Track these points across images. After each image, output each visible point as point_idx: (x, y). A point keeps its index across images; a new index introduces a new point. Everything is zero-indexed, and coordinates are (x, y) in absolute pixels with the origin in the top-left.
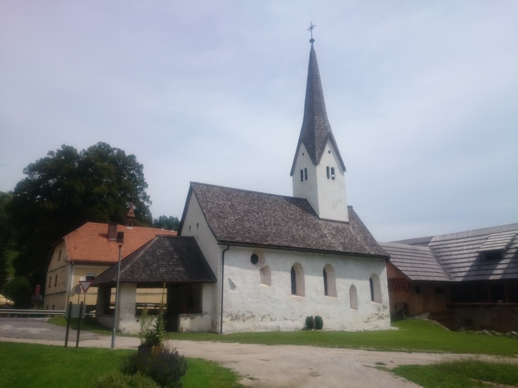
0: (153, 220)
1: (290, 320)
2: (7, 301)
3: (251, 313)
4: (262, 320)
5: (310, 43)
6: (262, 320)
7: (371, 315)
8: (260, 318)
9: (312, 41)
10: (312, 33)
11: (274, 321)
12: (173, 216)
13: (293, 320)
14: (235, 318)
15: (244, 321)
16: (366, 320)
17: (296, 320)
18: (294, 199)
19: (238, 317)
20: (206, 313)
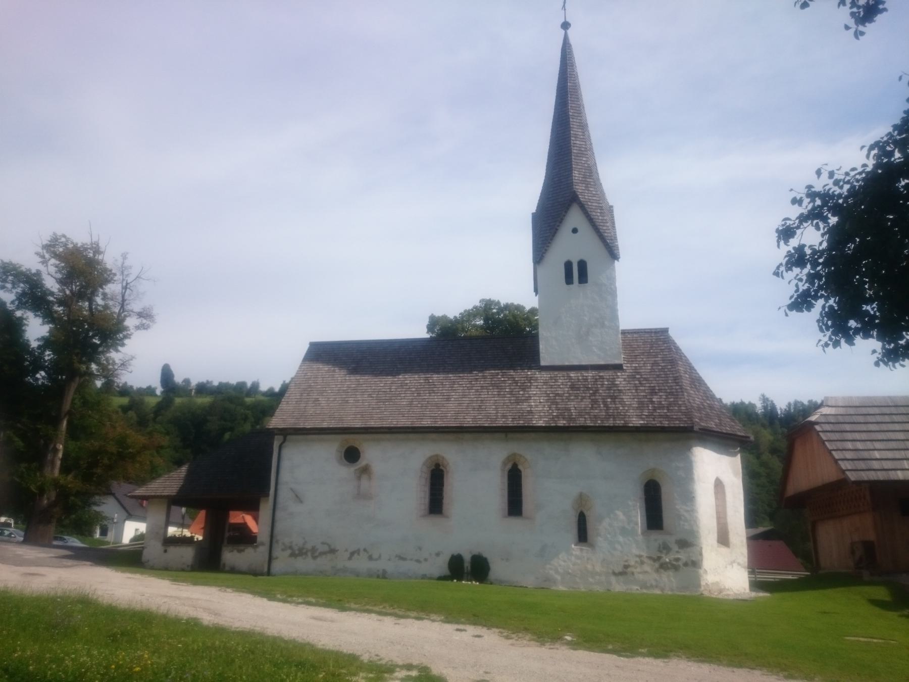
0: (779, 412)
1: (411, 560)
2: (182, 532)
3: (329, 546)
4: (350, 558)
5: (563, 30)
6: (350, 558)
7: (638, 559)
8: (347, 555)
9: (566, 26)
10: (566, 11)
11: (376, 560)
12: (814, 400)
13: (418, 561)
14: (299, 553)
15: (315, 558)
16: (619, 569)
17: (426, 560)
18: (645, 332)
19: (304, 551)
20: (262, 544)
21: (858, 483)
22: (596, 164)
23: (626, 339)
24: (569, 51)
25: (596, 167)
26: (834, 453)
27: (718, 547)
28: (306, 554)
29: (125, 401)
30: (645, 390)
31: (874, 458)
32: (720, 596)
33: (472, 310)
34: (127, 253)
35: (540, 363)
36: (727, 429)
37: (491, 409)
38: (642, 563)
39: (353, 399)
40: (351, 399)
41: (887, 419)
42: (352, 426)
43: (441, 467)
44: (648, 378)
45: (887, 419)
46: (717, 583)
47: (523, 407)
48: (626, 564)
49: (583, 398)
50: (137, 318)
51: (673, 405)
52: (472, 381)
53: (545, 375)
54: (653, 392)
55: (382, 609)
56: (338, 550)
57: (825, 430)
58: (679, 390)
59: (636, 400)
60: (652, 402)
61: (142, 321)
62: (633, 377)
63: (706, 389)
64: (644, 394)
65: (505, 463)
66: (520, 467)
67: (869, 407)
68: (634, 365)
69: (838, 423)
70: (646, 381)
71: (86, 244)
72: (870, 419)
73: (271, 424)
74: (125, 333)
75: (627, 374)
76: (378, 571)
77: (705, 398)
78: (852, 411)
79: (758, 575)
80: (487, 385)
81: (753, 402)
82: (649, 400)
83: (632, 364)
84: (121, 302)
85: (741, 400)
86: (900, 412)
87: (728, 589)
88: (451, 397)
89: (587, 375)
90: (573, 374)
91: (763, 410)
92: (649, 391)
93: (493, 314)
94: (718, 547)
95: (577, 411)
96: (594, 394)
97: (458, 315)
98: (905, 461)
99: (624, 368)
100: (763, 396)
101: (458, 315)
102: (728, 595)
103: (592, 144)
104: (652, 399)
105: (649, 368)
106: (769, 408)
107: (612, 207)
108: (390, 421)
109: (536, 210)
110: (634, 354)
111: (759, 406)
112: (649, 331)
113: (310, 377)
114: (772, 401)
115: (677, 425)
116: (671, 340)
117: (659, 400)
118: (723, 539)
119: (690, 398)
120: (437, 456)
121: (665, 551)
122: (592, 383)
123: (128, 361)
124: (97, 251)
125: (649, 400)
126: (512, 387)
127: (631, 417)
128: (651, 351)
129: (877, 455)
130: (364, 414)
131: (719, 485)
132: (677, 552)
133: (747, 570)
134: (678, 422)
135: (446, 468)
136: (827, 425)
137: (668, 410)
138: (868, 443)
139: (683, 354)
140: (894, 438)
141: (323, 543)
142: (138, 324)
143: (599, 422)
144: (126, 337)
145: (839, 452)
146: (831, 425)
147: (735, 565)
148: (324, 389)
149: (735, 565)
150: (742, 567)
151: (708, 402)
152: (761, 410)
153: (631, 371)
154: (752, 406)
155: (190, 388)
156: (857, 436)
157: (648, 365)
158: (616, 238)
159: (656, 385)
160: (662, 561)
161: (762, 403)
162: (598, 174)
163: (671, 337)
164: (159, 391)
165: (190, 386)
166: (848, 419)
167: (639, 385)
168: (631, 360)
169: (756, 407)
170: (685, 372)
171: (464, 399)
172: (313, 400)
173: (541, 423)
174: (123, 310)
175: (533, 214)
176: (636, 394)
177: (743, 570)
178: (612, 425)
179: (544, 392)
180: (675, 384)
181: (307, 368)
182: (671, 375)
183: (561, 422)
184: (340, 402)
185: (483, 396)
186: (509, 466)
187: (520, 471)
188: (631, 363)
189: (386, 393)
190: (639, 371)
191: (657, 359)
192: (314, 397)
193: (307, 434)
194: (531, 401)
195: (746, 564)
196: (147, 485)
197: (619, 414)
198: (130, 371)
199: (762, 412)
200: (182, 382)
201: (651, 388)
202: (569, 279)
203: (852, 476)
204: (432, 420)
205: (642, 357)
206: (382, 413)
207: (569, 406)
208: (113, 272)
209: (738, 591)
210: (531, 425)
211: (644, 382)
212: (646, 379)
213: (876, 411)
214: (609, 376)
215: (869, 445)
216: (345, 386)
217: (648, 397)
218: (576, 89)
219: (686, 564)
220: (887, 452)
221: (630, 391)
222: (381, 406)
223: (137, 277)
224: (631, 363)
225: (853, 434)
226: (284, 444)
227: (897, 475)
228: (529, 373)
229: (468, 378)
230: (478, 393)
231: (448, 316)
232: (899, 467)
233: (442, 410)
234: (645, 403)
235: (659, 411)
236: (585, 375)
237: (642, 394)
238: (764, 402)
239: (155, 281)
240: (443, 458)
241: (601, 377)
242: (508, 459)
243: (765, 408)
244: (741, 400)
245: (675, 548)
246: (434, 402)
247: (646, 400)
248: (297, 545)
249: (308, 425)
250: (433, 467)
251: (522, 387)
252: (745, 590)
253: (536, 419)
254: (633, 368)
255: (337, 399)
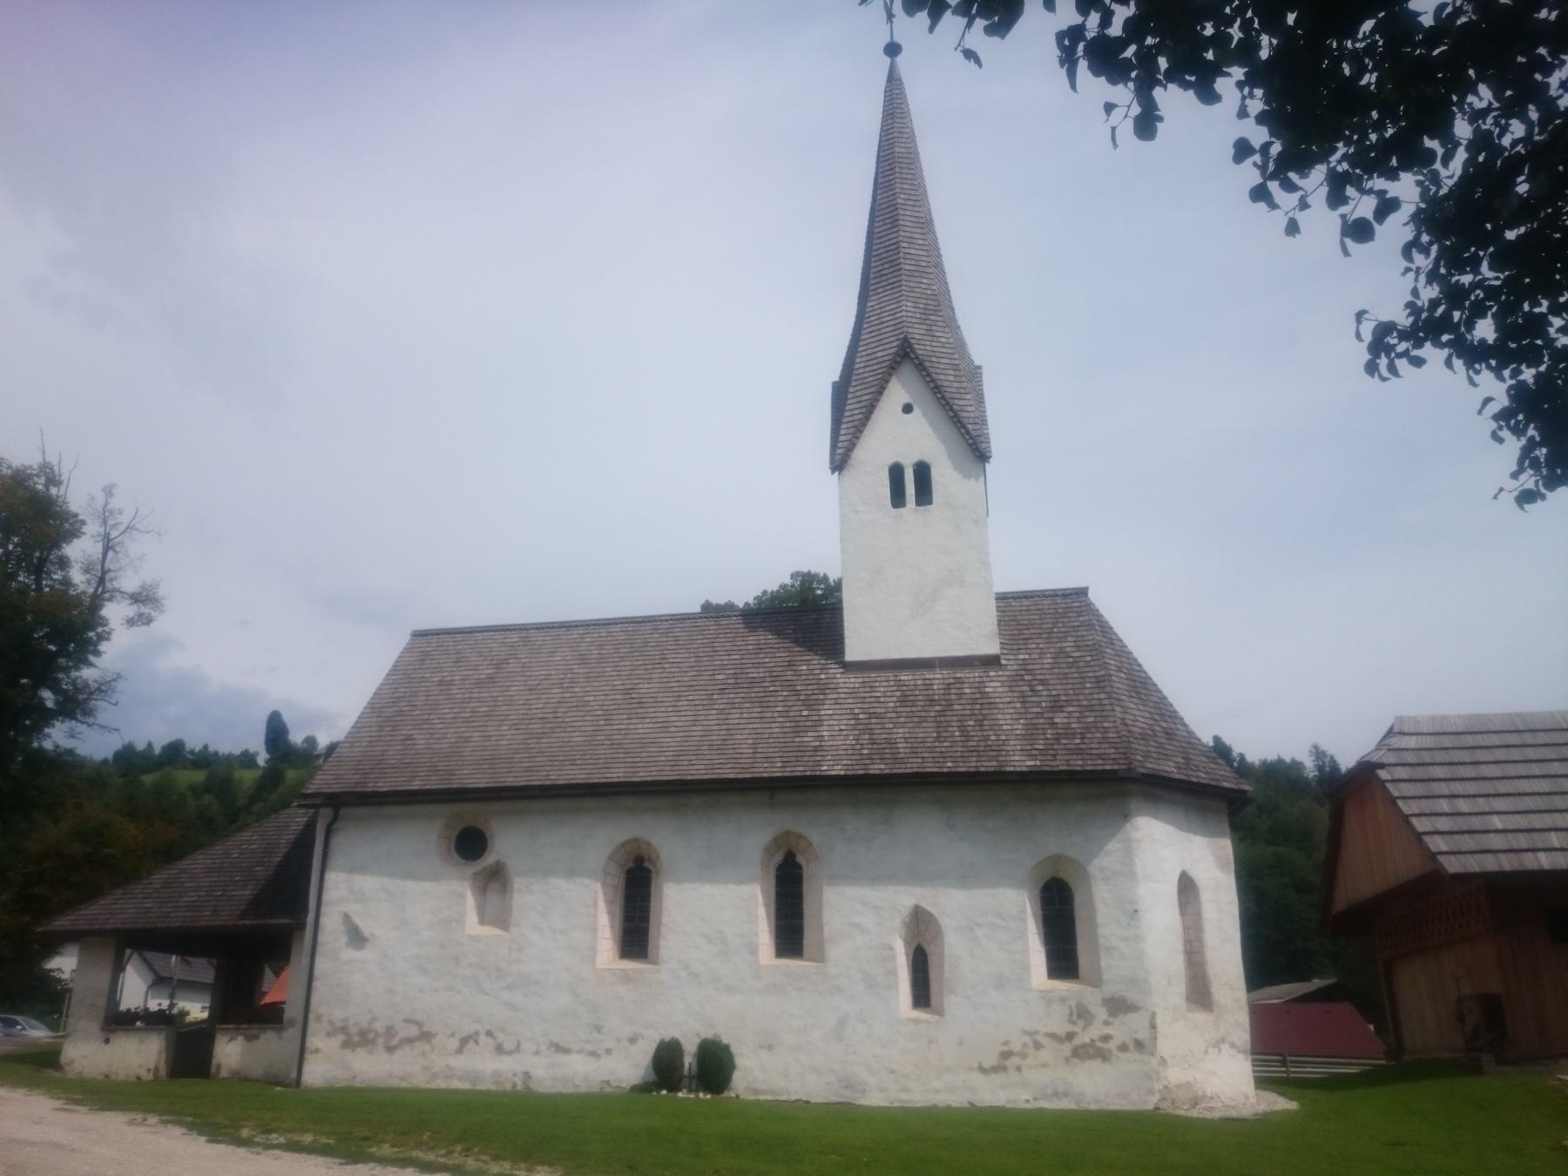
3: (419, 1024)
6: (460, 1051)
7: (1028, 1039)
8: (454, 1044)
11: (510, 1053)
13: (593, 1054)
14: (358, 1039)
15: (390, 1049)
16: (990, 1060)
17: (609, 1051)
19: (371, 1036)
21: (1462, 878)
22: (949, 291)
23: (1009, 609)
24: (898, 92)
25: (949, 296)
26: (1414, 821)
27: (1189, 1010)
28: (373, 1041)
29: (199, 777)
30: (1041, 702)
31: (1493, 828)
32: (1194, 1113)
33: (778, 591)
34: (114, 485)
35: (843, 656)
36: (1202, 777)
37: (745, 746)
38: (1038, 1046)
39: (480, 734)
40: (475, 734)
41: (1516, 754)
42: (471, 786)
43: (646, 864)
44: (1046, 679)
45: (1516, 754)
46: (1189, 1085)
47: (806, 739)
48: (1006, 1048)
49: (924, 720)
50: (131, 604)
51: (1093, 730)
52: (713, 694)
53: (853, 680)
54: (1056, 706)
55: (442, 1156)
56: (437, 1034)
57: (1396, 777)
58: (1106, 702)
59: (1022, 721)
60: (1053, 724)
61: (139, 609)
62: (1017, 678)
63: (1158, 700)
64: (1038, 710)
65: (769, 852)
66: (800, 859)
67: (1481, 733)
68: (1021, 657)
69: (1423, 764)
70: (1043, 685)
71: (30, 467)
72: (1481, 755)
73: (311, 786)
74: (100, 630)
75: (1007, 673)
76: (515, 1075)
77: (1157, 717)
78: (1447, 741)
79: (1292, 1067)
80: (740, 700)
81: (1299, 758)
82: (1047, 721)
83: (1018, 654)
84: (99, 575)
85: (1279, 756)
86: (1541, 742)
87: (1212, 1098)
88: (670, 724)
89: (932, 676)
90: (905, 677)
91: (1317, 773)
92: (1049, 704)
93: (815, 596)
94: (1189, 1010)
95: (909, 745)
96: (942, 713)
97: (751, 601)
98: (1553, 834)
99: (1003, 662)
100: (1316, 747)
101: (751, 601)
102: (1211, 1109)
103: (941, 256)
104: (1052, 718)
105: (1050, 661)
106: (1328, 769)
107: (980, 367)
108: (544, 773)
109: (840, 377)
110: (1022, 637)
111: (1309, 763)
112: (1051, 593)
113: (401, 695)
114: (1332, 757)
115: (1100, 768)
116: (1092, 610)
117: (1066, 720)
118: (1199, 993)
119: (1127, 716)
120: (637, 840)
121: (1081, 1023)
122: (942, 692)
123: (109, 682)
124: (53, 480)
125: (1047, 721)
126: (789, 704)
127: (1011, 753)
128: (1055, 630)
129: (1497, 822)
130: (497, 761)
131: (1187, 887)
132: (1106, 1023)
133: (1250, 1057)
134: (1100, 762)
135: (655, 866)
136: (1400, 768)
137: (1083, 738)
138: (1481, 800)
139: (1116, 635)
140: (1530, 791)
141: (407, 1021)
142: (131, 614)
143: (950, 764)
144: (101, 638)
145: (1423, 818)
146: (1407, 768)
147: (1225, 1047)
148: (426, 717)
149: (1225, 1047)
150: (1239, 1052)
151: (1164, 725)
152: (1313, 771)
153: (1015, 667)
154: (1296, 766)
155: (316, 753)
156: (1457, 788)
157: (1049, 656)
158: (984, 422)
159: (1061, 692)
160: (1078, 1041)
161: (1314, 761)
162: (953, 309)
163: (1094, 605)
164: (262, 759)
165: (316, 749)
166: (1440, 757)
167: (1030, 694)
168: (1015, 647)
169: (1305, 768)
170: (1120, 667)
171: (694, 728)
172: (402, 737)
173: (838, 770)
174: (103, 589)
175: (834, 383)
176: (1022, 711)
177: (1242, 1056)
178: (973, 770)
179: (848, 711)
180: (1097, 690)
181: (401, 679)
182: (1091, 674)
183: (876, 767)
184: (453, 740)
185: (731, 722)
186: (779, 858)
187: (800, 867)
188: (1016, 652)
189: (545, 721)
190: (1030, 667)
191: (1065, 644)
192: (404, 732)
193: (380, 804)
194: (823, 728)
195: (1248, 1046)
196: (67, 915)
197: (988, 748)
198: (114, 702)
199: (1316, 776)
200: (302, 743)
201: (1052, 699)
202: (898, 498)
203: (1452, 865)
204: (627, 770)
205: (1037, 641)
206: (532, 759)
207: (894, 736)
208: (81, 517)
209: (1233, 1100)
210: (818, 773)
211: (1040, 688)
212: (1043, 682)
213: (1494, 740)
214: (974, 677)
215: (1482, 805)
216: (468, 710)
217: (1046, 715)
218: (913, 159)
219: (1123, 1048)
220: (1517, 816)
221: (1012, 705)
222: (533, 746)
223: (128, 528)
224: (1016, 652)
225: (1452, 784)
226: (335, 826)
227: (1537, 860)
228: (823, 676)
229: (705, 688)
230: (723, 717)
231: (736, 603)
232: (1540, 845)
233: (649, 749)
234: (1040, 726)
235: (1065, 741)
236: (927, 676)
237: (1035, 710)
238: (1318, 758)
239: (160, 535)
240: (648, 844)
241: (959, 681)
242: (776, 843)
243: (1320, 768)
244: (1279, 756)
245: (1101, 1014)
246: (637, 736)
247: (1042, 721)
248: (356, 1024)
249: (384, 786)
250: (631, 865)
251: (807, 703)
252: (1247, 1097)
253: (828, 763)
254: (1020, 662)
255: (449, 736)
